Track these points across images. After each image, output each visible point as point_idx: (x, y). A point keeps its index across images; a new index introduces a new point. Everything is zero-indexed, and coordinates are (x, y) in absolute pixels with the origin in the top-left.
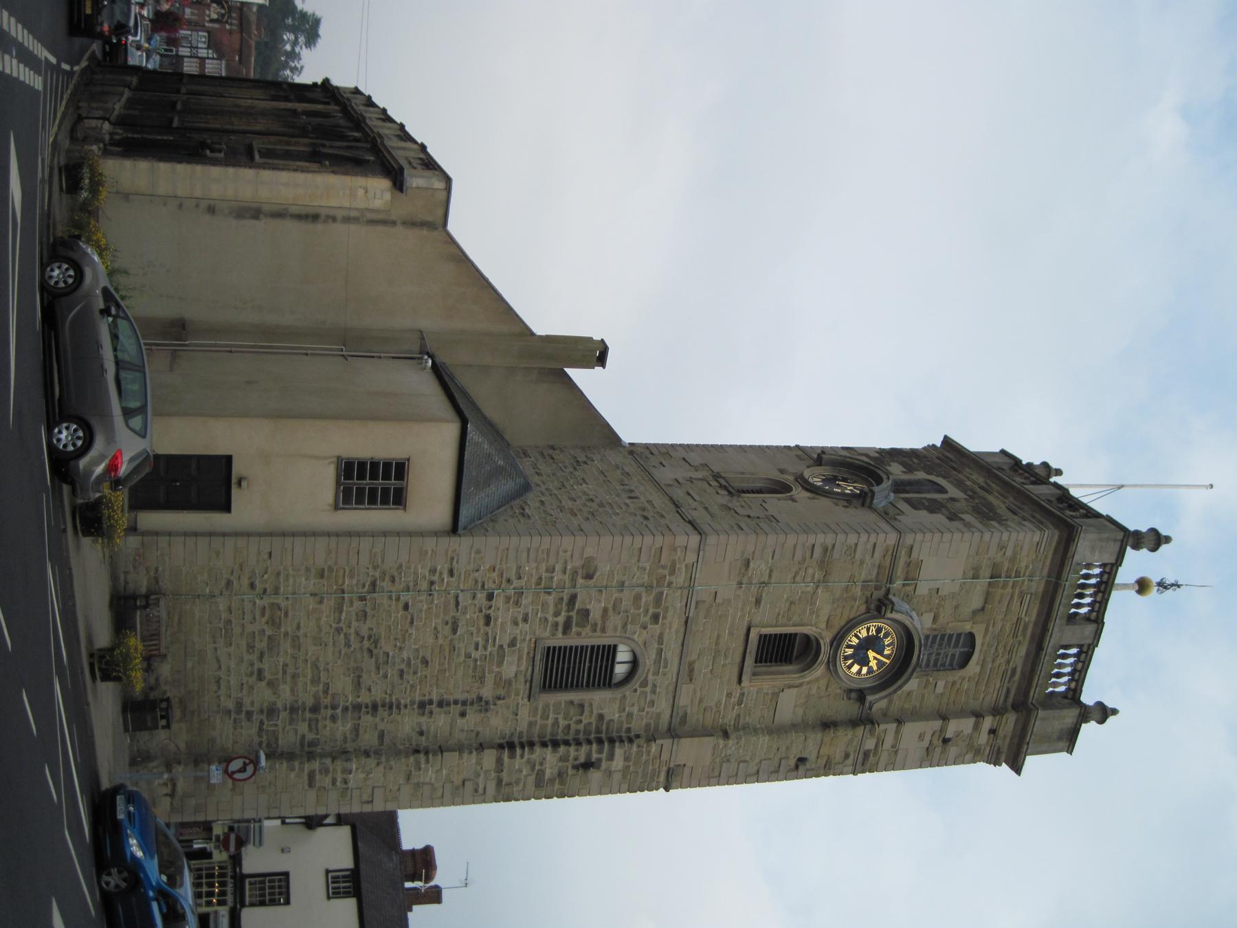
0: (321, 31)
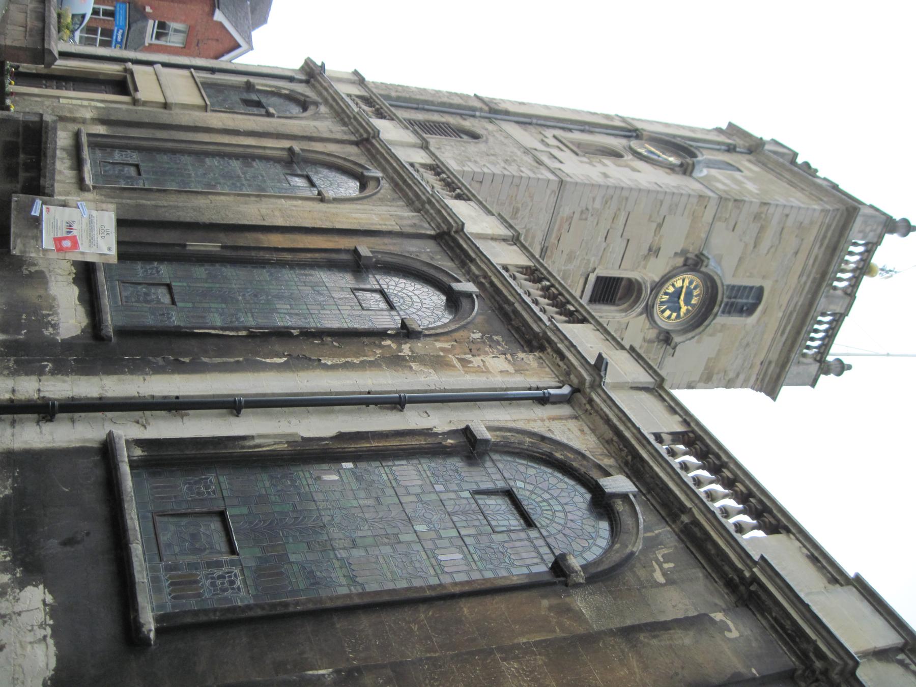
0: (813, 166)
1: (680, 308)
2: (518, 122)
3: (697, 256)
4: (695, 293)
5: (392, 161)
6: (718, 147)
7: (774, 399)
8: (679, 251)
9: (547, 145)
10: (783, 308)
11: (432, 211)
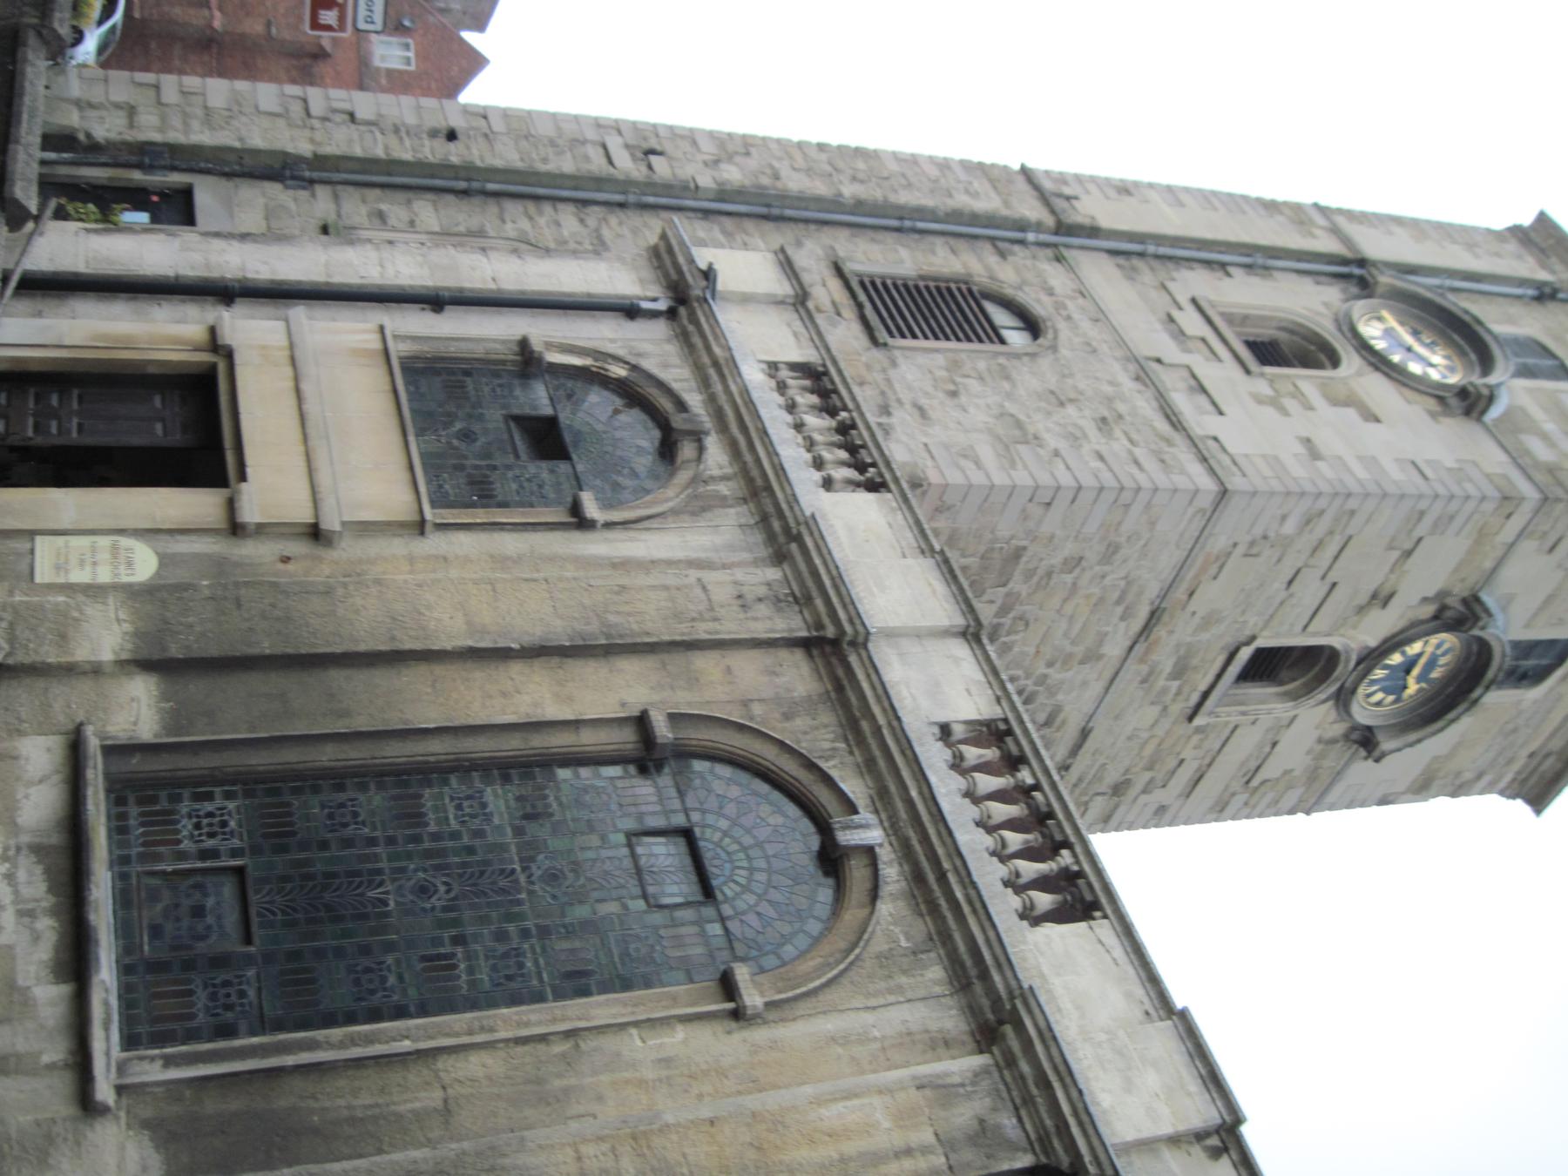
1: (1405, 687)
3: (1465, 601)
4: (1442, 661)
5: (906, 774)
8: (1431, 593)
9: (1180, 335)
11: (1025, 1067)
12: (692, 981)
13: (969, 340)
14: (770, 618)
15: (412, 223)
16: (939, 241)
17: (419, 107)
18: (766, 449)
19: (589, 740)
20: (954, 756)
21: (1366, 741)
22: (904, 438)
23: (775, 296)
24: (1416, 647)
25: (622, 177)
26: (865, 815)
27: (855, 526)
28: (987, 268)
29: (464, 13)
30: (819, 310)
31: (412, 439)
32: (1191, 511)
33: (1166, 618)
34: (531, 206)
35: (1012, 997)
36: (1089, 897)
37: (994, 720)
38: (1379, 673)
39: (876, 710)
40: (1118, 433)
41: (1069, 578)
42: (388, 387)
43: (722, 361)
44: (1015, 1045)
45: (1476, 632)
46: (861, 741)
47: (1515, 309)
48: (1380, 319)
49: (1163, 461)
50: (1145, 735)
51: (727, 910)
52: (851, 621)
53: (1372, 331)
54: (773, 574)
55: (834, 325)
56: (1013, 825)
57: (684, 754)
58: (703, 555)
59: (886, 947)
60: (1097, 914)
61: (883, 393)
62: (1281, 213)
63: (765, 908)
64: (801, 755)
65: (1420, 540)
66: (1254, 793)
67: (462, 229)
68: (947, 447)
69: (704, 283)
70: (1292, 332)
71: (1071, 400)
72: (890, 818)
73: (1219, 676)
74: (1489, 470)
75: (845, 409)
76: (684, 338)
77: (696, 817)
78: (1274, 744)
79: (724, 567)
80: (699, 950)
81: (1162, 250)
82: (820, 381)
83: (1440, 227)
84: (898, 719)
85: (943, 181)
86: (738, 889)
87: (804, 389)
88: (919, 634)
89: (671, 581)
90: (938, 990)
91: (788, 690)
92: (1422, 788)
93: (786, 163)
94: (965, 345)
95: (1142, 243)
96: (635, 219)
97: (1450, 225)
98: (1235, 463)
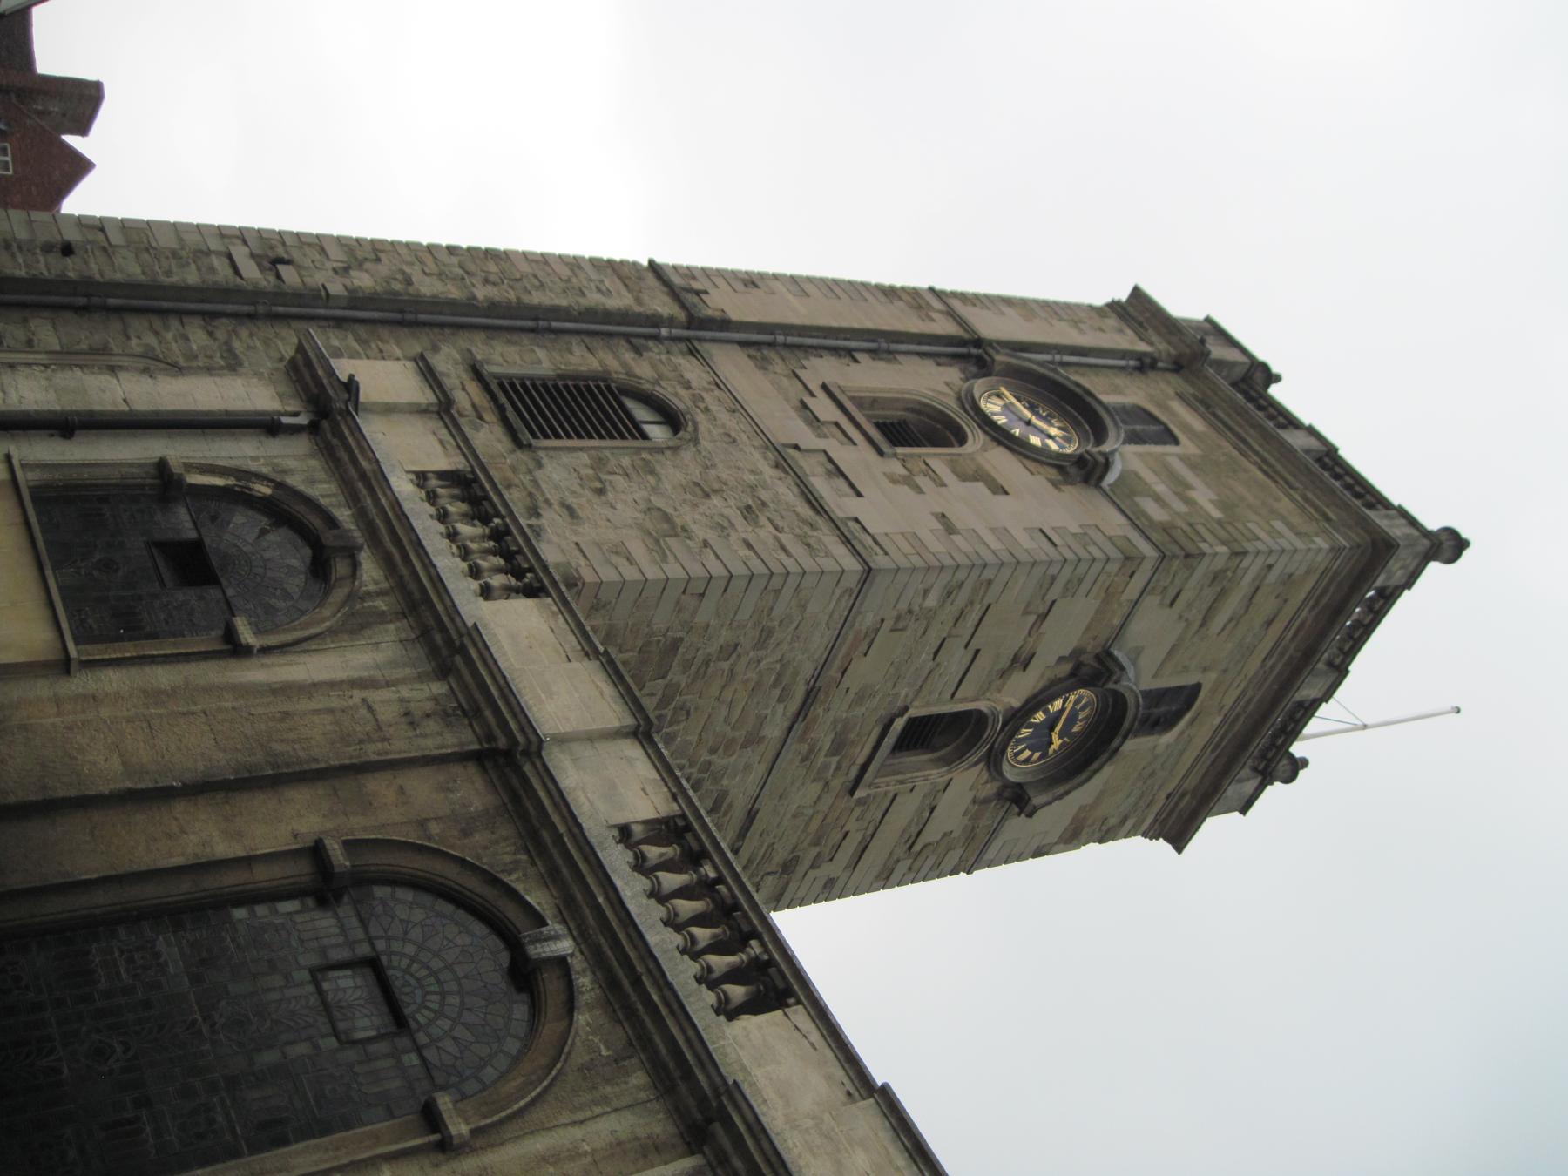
1: (1051, 743)
2: (743, 344)
3: (1097, 657)
5: (590, 880)
6: (1122, 363)
7: (1179, 849)
9: (814, 421)
10: (1226, 709)
12: (392, 1116)
13: (612, 437)
14: (440, 734)
15: (30, 343)
16: (574, 340)
17: (30, 222)
18: (422, 561)
19: (263, 875)
20: (636, 857)
21: (1017, 799)
22: (555, 539)
23: (419, 405)
24: (1058, 704)
25: (250, 288)
26: (554, 926)
27: (517, 632)
28: (624, 364)
29: (64, 115)
30: (461, 415)
31: (49, 572)
32: (838, 592)
33: (822, 696)
34: (157, 322)
35: (718, 1096)
36: (780, 985)
37: (674, 817)
38: (1025, 732)
39: (556, 819)
40: (763, 520)
41: (726, 666)
42: (19, 520)
43: (369, 474)
44: (726, 1143)
45: (1111, 686)
46: (542, 850)
47: (1120, 380)
48: (999, 396)
49: (808, 545)
50: (810, 811)
51: (422, 1038)
52: (522, 730)
53: (992, 407)
54: (438, 688)
55: (477, 429)
56: (700, 920)
57: (363, 880)
58: (365, 674)
59: (587, 1058)
60: (791, 1001)
61: (530, 494)
62: (900, 299)
63: (460, 1032)
64: (484, 871)
65: (1054, 602)
66: (918, 858)
67: (84, 346)
68: (598, 545)
69: (346, 396)
70: (918, 412)
71: (715, 491)
72: (578, 927)
73: (876, 748)
74: (1112, 533)
75: (498, 515)
76: (328, 453)
77: (381, 945)
78: (932, 810)
79: (388, 684)
80: (397, 1083)
81: (790, 339)
82: (469, 489)
83: (1046, 306)
84: (579, 826)
85: (574, 280)
86: (432, 1015)
87: (454, 497)
88: (591, 738)
89: (335, 703)
90: (643, 1095)
91: (464, 805)
92: (1072, 837)
93: (417, 267)
94: (608, 443)
95: (772, 333)
96: (267, 330)
97: (1056, 303)
98: (876, 542)
